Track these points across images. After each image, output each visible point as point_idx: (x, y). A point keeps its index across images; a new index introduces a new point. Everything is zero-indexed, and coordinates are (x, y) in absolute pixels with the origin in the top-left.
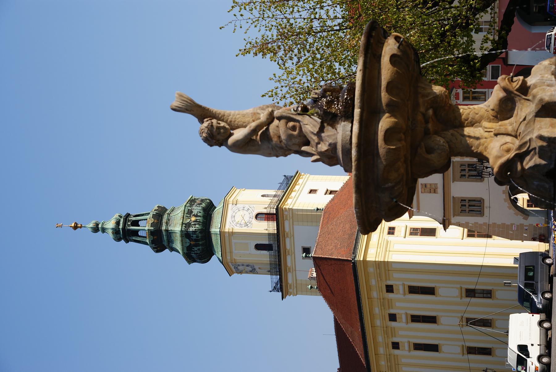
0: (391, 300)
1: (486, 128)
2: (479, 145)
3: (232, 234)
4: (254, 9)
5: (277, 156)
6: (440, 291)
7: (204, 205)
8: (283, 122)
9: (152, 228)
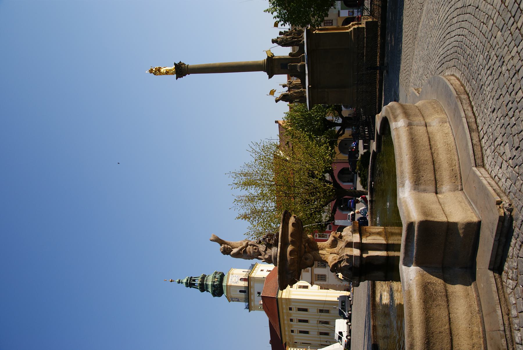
2: (325, 257)
4: (242, 203)
5: (249, 259)
6: (310, 310)
7: (220, 274)
8: (252, 246)
9: (200, 283)
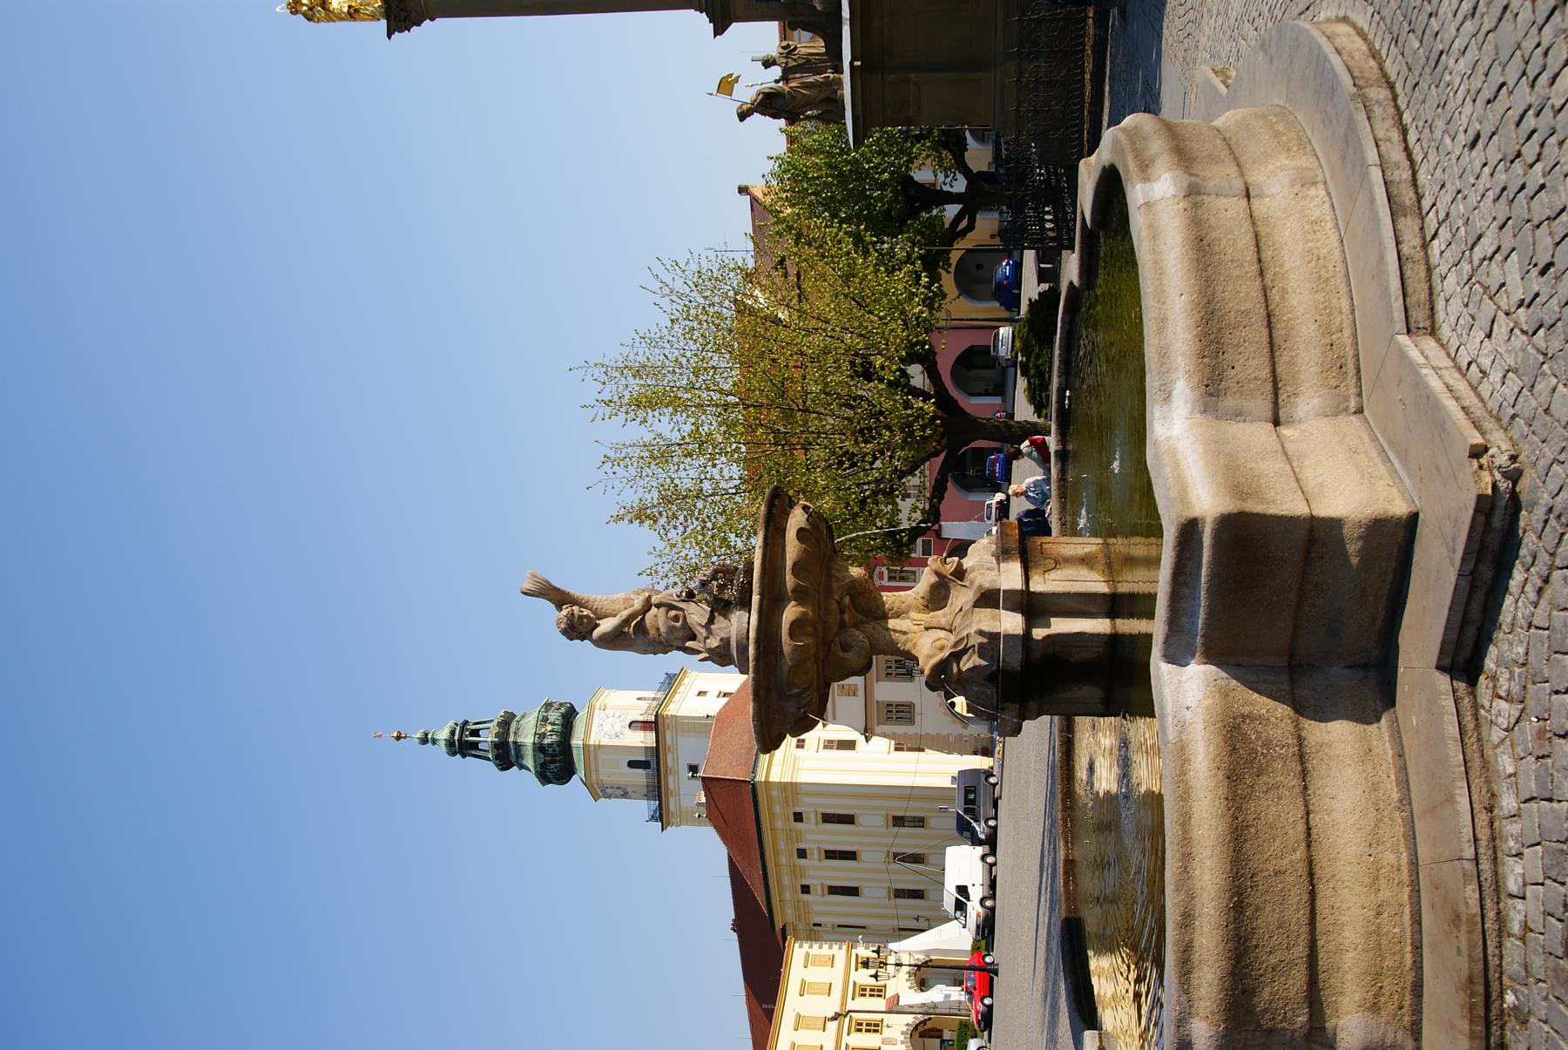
0: (804, 867)
1: (915, 620)
2: (907, 641)
3: (599, 747)
5: (655, 654)
7: (563, 710)
8: (663, 610)
9: (497, 740)
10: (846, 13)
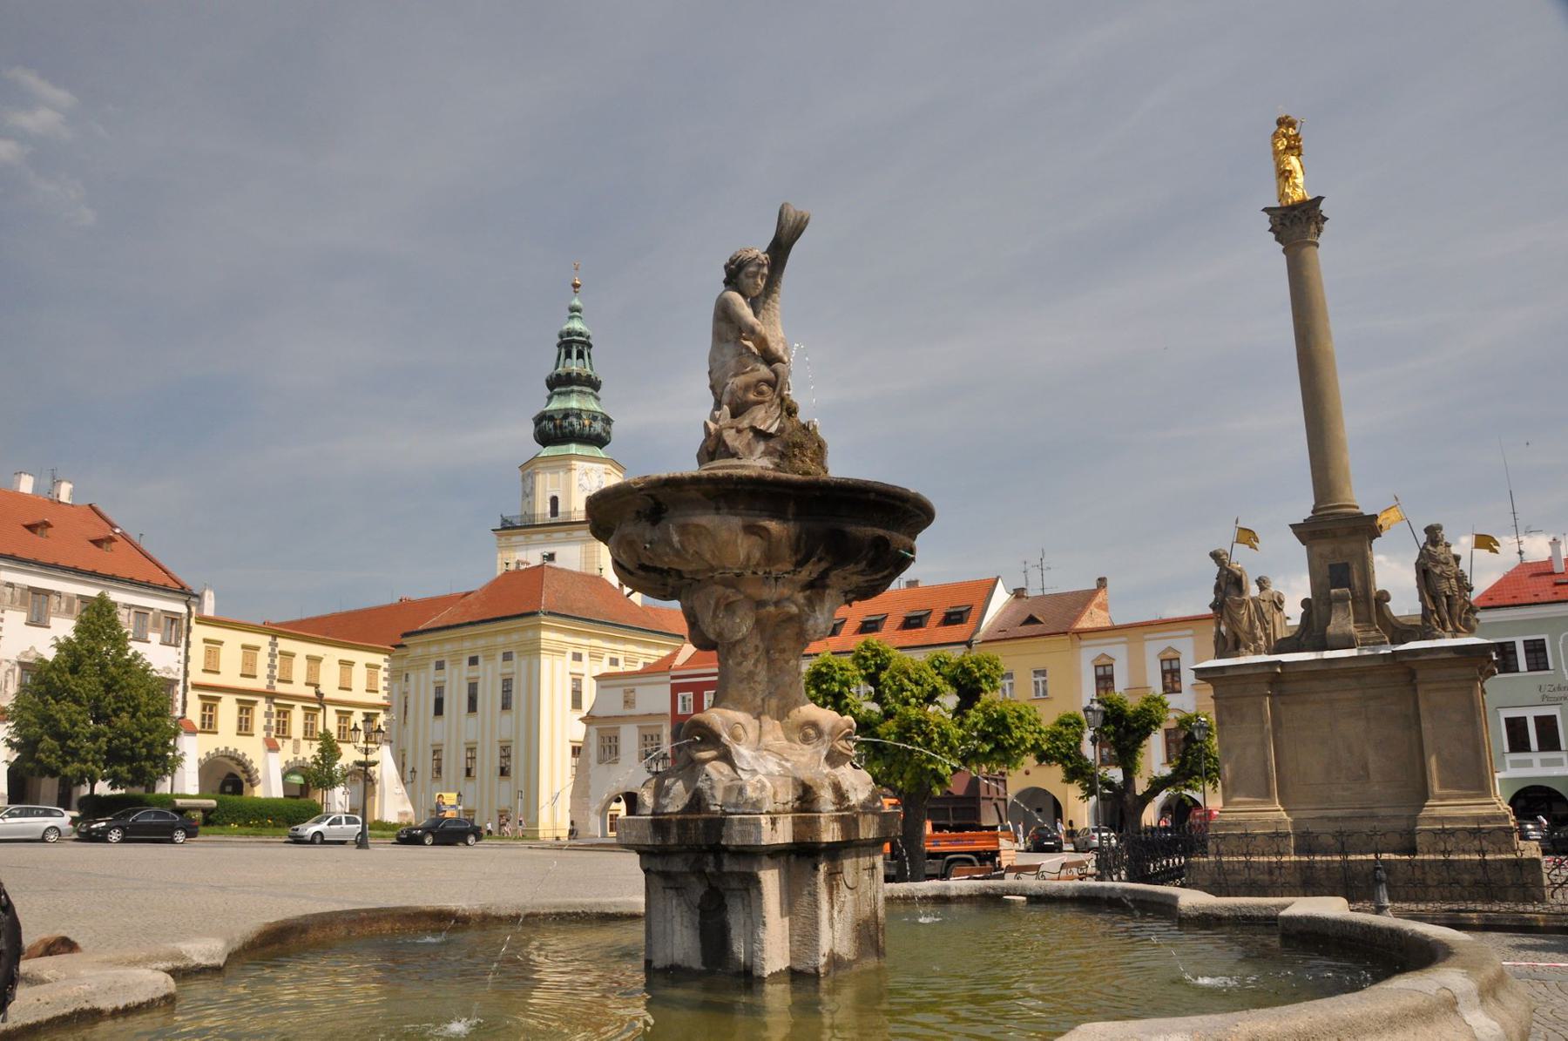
10: (1328, 654)
